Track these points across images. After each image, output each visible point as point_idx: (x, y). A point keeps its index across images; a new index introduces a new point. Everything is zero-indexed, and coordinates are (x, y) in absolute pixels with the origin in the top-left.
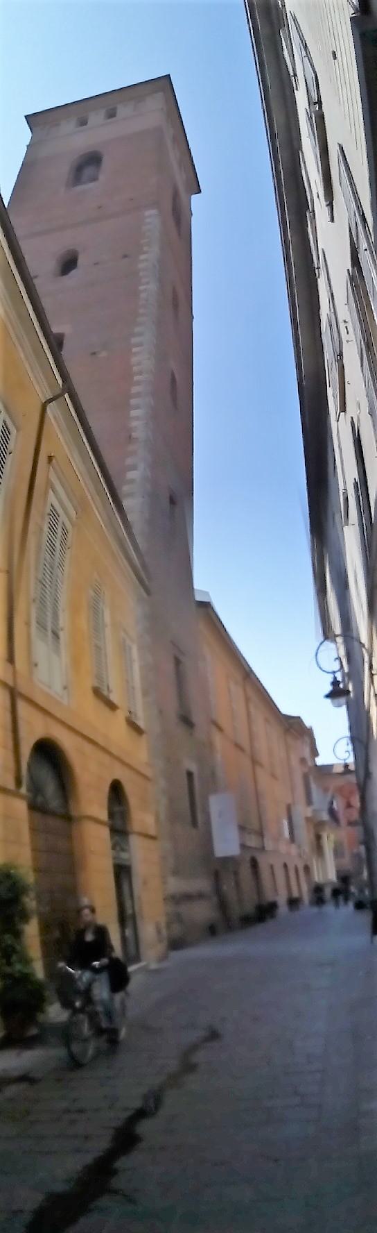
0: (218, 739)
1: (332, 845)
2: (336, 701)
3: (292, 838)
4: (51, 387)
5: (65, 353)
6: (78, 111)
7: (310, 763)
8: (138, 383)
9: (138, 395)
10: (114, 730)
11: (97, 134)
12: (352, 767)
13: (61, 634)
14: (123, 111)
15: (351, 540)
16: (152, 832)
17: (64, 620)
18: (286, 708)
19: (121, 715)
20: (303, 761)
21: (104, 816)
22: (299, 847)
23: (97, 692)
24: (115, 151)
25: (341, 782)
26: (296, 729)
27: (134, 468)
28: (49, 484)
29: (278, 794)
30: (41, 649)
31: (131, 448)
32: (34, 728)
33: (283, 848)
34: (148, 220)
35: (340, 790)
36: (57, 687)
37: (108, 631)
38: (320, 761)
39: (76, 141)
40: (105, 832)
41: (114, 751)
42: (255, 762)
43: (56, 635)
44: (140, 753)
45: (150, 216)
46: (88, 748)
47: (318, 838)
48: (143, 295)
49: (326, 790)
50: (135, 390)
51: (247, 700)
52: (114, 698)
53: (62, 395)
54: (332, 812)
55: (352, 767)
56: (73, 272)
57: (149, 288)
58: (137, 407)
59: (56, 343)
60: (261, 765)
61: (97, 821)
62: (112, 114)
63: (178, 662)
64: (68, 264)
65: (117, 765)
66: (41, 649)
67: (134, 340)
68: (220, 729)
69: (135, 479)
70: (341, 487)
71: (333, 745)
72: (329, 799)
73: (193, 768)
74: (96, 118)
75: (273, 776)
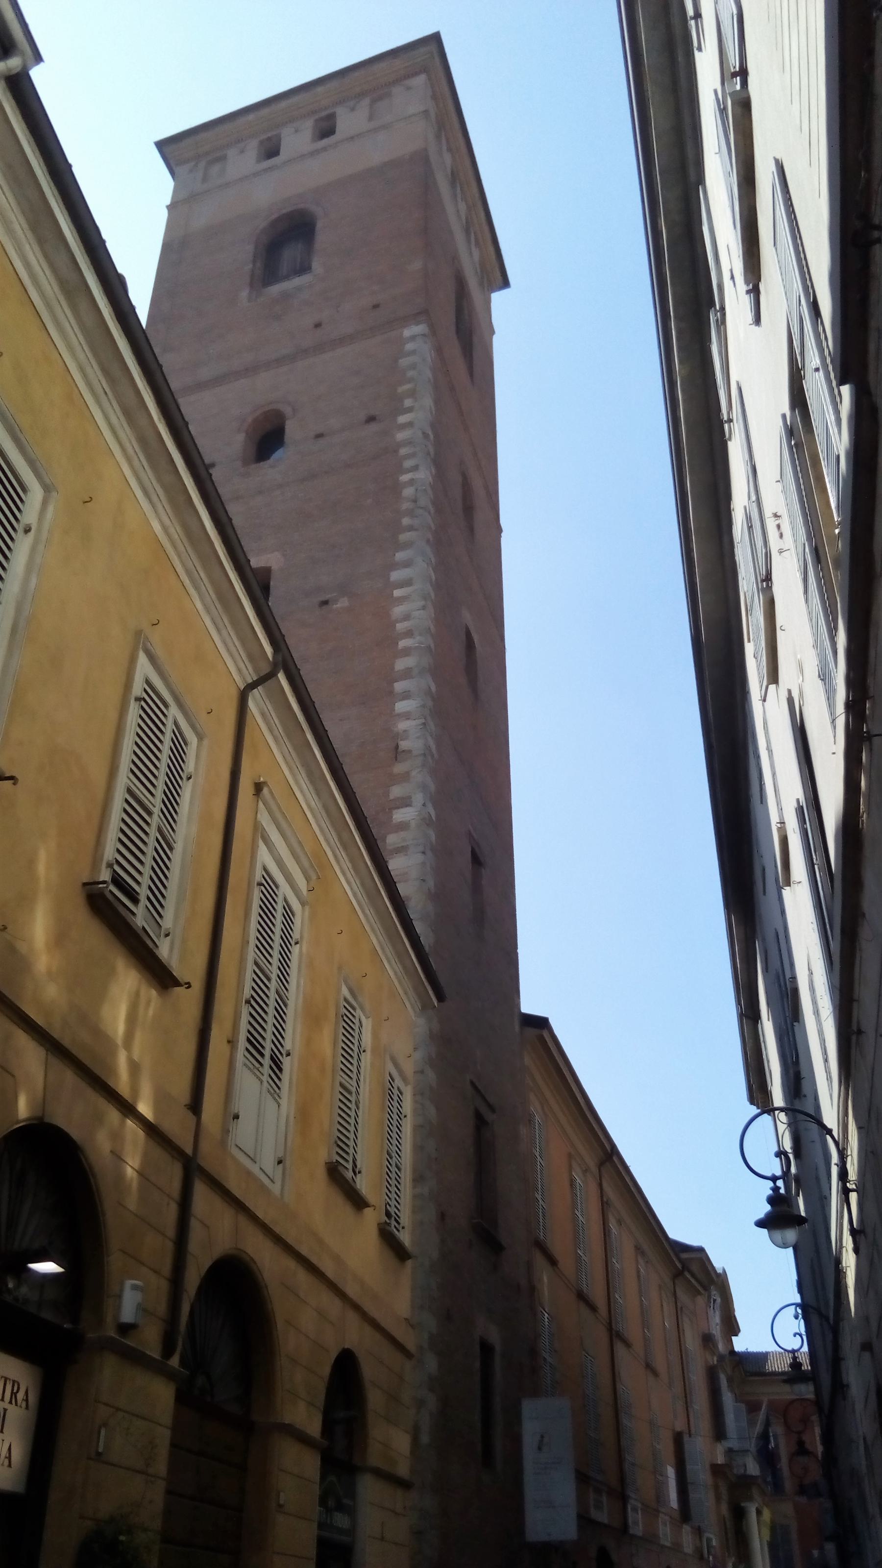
0: (545, 1278)
1: (766, 1534)
2: (778, 1235)
3: (685, 1513)
5: (275, 602)
6: (258, 128)
7: (721, 1347)
8: (406, 652)
9: (407, 674)
10: (353, 1248)
11: (303, 173)
12: (806, 1366)
13: (286, 1062)
14: (349, 121)
15: (799, 912)
16: (403, 1470)
17: (293, 1039)
18: (679, 1227)
19: (371, 1218)
20: (707, 1340)
21: (314, 1427)
22: (699, 1532)
23: (334, 1172)
25: (786, 1393)
26: (694, 1275)
27: (405, 802)
28: (258, 831)
29: (658, 1407)
30: (249, 1087)
31: (399, 768)
32: (216, 1232)
33: (665, 1532)
34: (409, 347)
35: (783, 1410)
36: (268, 1161)
37: (367, 1059)
38: (740, 1344)
39: (267, 193)
41: (352, 1290)
42: (615, 1335)
43: (277, 1065)
44: (397, 1298)
45: (413, 338)
46: (302, 1277)
47: (739, 1514)
48: (408, 492)
49: (753, 1408)
50: (401, 664)
51: (605, 1205)
52: (363, 1185)
53: (272, 675)
54: (768, 1457)
55: (806, 1366)
56: (278, 454)
57: (417, 477)
58: (406, 695)
59: (259, 585)
60: (628, 1345)
61: (303, 1439)
62: (326, 129)
63: (480, 1122)
64: (268, 439)
65: (352, 1317)
66: (249, 1087)
67: (396, 576)
68: (553, 1262)
69: (408, 817)
70: (774, 819)
71: (767, 1315)
72: (758, 1428)
73: (495, 1336)
74: (297, 140)
75: (649, 1367)
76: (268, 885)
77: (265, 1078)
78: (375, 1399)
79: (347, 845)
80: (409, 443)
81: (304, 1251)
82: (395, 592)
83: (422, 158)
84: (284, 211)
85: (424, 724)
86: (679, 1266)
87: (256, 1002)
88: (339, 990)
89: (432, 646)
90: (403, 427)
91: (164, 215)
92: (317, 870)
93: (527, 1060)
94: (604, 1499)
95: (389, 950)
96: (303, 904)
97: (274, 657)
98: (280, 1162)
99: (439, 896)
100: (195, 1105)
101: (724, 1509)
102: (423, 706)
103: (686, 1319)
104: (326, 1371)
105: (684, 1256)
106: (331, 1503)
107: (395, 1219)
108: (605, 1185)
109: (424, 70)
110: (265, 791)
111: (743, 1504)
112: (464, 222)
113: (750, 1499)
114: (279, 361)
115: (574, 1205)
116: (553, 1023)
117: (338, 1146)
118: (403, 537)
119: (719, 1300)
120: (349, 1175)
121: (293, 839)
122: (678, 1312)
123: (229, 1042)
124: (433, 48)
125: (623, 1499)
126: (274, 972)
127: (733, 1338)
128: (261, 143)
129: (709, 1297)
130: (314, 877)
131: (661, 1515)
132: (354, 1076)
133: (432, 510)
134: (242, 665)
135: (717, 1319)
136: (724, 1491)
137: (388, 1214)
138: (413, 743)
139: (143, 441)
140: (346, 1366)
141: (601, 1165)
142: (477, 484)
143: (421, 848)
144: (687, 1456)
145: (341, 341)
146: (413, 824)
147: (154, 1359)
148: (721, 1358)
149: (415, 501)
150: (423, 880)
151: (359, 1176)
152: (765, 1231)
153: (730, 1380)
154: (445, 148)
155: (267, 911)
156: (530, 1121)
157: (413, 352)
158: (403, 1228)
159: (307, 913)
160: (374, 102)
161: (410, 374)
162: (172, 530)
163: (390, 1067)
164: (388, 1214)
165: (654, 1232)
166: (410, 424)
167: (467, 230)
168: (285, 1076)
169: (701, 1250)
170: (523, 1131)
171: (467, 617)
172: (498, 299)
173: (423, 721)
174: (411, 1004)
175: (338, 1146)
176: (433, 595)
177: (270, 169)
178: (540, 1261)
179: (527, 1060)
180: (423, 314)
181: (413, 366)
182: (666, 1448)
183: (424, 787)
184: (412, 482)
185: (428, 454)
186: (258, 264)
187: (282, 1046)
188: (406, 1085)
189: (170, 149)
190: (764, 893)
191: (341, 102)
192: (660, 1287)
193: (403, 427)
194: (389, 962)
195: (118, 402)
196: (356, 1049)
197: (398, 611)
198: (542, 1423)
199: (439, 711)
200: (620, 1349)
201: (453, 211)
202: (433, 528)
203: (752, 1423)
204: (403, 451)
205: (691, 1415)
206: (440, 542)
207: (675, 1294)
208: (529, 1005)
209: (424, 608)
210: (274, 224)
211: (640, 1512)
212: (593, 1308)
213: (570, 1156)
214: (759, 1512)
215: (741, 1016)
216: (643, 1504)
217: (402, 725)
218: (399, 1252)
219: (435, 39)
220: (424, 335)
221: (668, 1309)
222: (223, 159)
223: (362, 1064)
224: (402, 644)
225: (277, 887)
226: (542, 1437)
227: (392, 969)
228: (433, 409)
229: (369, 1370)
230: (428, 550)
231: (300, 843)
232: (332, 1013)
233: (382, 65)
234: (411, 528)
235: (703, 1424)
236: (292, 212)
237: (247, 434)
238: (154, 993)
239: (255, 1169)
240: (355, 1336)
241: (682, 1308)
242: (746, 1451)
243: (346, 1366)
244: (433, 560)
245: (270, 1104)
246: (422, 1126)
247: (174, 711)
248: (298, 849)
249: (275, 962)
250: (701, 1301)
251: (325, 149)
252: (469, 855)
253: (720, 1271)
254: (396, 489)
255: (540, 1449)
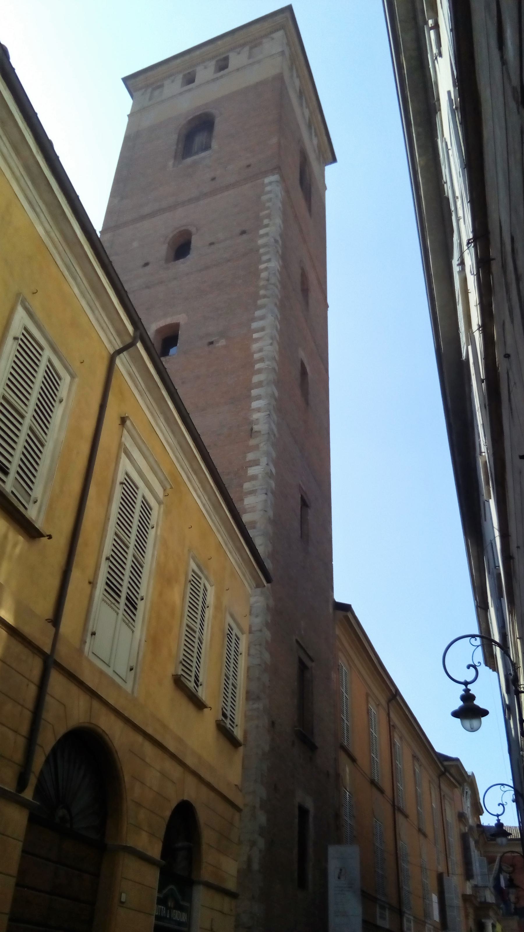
0: (347, 770)
2: (467, 723)
4: (119, 333)
6: (183, 67)
8: (259, 371)
9: (260, 384)
10: (198, 737)
13: (141, 605)
14: (236, 60)
16: (231, 885)
19: (210, 717)
20: (461, 816)
21: (155, 851)
24: (231, 120)
27: (256, 463)
28: (122, 448)
29: (425, 857)
30: (106, 617)
31: (253, 442)
32: (67, 709)
34: (268, 188)
36: (122, 670)
37: (209, 613)
38: (487, 820)
39: (185, 103)
40: (151, 877)
41: (190, 761)
42: (396, 809)
43: (132, 604)
44: (231, 772)
45: (270, 183)
46: (148, 749)
48: (264, 275)
49: (491, 861)
50: (256, 379)
51: (391, 727)
52: (203, 693)
57: (270, 265)
58: (259, 398)
62: (223, 65)
63: (303, 667)
65: (190, 780)
68: (353, 760)
73: (309, 804)
74: (205, 73)
76: (129, 486)
77: (121, 612)
78: (208, 836)
79: (197, 472)
80: (265, 245)
81: (150, 731)
82: (254, 335)
83: (280, 78)
84: (196, 114)
85: (269, 414)
86: (443, 769)
87: (116, 561)
88: (188, 564)
89: (277, 368)
90: (263, 236)
91: (126, 120)
92: (173, 485)
93: (338, 632)
94: (387, 913)
95: (231, 545)
96: (160, 503)
97: (134, 334)
98: (131, 669)
99: (276, 522)
100: (56, 620)
101: (471, 923)
102: (269, 404)
103: (446, 802)
104: (168, 814)
105: (446, 763)
106: (170, 904)
107: (230, 719)
108: (392, 715)
109: (282, 27)
110: (128, 423)
111: (483, 921)
112: (307, 121)
113: (488, 917)
114: (190, 201)
115: (369, 726)
116: (354, 607)
117: (183, 665)
118: (260, 302)
119: (469, 792)
120: (191, 685)
121: (148, 456)
122: (442, 798)
123: (90, 583)
124: (288, 14)
125: (400, 913)
126: (132, 542)
127: (480, 816)
128: (185, 76)
129: (463, 789)
130: (168, 487)
131: (427, 925)
132: (198, 621)
133: (279, 286)
134: (112, 338)
135: (469, 804)
136: (471, 911)
137: (224, 715)
138: (262, 427)
139: (27, 168)
140: (184, 813)
141: (389, 701)
142: (312, 277)
143: (264, 491)
144: (446, 887)
145: (227, 187)
146: (260, 476)
147: (10, 792)
148: (471, 828)
149: (268, 280)
150: (266, 511)
151: (200, 688)
152: (458, 720)
153: (477, 842)
154: (295, 75)
155: (128, 502)
156: (339, 669)
157: (270, 192)
158: (237, 726)
159: (162, 509)
160: (251, 48)
161: (268, 204)
162: (53, 235)
163: (229, 620)
164: (224, 715)
165: (425, 746)
166: (267, 234)
167: (310, 126)
168: (140, 613)
169: (457, 760)
170: (334, 676)
171: (302, 354)
172: (330, 170)
173: (268, 413)
174: (248, 583)
175: (183, 665)
176: (278, 337)
177: (190, 90)
178: (343, 758)
179: (338, 632)
180: (278, 169)
181: (270, 200)
182: (432, 883)
183: (268, 454)
184: (266, 269)
185: (278, 252)
186: (180, 146)
187: (138, 593)
188: (243, 634)
189: (131, 82)
190: (485, 520)
191: (232, 49)
192: (430, 782)
193: (263, 236)
194: (230, 552)
195: (8, 139)
196: (200, 604)
197: (255, 346)
198: (342, 861)
199: (279, 408)
200: (400, 819)
201: (301, 114)
202: (280, 297)
203: (490, 870)
204: (262, 251)
205: (450, 864)
206: (283, 306)
207: (440, 787)
208: (339, 596)
209: (271, 344)
210: (190, 122)
211: (412, 923)
212: (382, 791)
213: (367, 695)
214: (494, 926)
215: (477, 607)
216: (414, 917)
217: (255, 416)
218: (234, 743)
219: (289, 9)
220: (277, 182)
221: (435, 794)
222: (161, 86)
223: (207, 615)
224: (257, 366)
225: (137, 488)
226: (341, 870)
227: (233, 559)
228: (282, 226)
229: (203, 816)
230: (276, 311)
231: (156, 461)
232: (182, 579)
233: (258, 26)
234: (265, 296)
235: (457, 869)
236: (200, 114)
237: (169, 244)
238: (21, 538)
239: (109, 672)
240: (192, 792)
241: (444, 796)
242: (486, 887)
243: (184, 813)
244: (279, 316)
245: (125, 630)
246: (260, 665)
247: (47, 353)
248: (156, 467)
249: (133, 536)
250: (457, 792)
251: (222, 77)
252: (299, 500)
253: (469, 774)
254: (256, 274)
255: (339, 878)
